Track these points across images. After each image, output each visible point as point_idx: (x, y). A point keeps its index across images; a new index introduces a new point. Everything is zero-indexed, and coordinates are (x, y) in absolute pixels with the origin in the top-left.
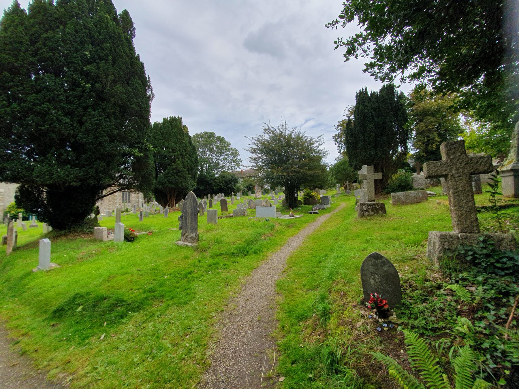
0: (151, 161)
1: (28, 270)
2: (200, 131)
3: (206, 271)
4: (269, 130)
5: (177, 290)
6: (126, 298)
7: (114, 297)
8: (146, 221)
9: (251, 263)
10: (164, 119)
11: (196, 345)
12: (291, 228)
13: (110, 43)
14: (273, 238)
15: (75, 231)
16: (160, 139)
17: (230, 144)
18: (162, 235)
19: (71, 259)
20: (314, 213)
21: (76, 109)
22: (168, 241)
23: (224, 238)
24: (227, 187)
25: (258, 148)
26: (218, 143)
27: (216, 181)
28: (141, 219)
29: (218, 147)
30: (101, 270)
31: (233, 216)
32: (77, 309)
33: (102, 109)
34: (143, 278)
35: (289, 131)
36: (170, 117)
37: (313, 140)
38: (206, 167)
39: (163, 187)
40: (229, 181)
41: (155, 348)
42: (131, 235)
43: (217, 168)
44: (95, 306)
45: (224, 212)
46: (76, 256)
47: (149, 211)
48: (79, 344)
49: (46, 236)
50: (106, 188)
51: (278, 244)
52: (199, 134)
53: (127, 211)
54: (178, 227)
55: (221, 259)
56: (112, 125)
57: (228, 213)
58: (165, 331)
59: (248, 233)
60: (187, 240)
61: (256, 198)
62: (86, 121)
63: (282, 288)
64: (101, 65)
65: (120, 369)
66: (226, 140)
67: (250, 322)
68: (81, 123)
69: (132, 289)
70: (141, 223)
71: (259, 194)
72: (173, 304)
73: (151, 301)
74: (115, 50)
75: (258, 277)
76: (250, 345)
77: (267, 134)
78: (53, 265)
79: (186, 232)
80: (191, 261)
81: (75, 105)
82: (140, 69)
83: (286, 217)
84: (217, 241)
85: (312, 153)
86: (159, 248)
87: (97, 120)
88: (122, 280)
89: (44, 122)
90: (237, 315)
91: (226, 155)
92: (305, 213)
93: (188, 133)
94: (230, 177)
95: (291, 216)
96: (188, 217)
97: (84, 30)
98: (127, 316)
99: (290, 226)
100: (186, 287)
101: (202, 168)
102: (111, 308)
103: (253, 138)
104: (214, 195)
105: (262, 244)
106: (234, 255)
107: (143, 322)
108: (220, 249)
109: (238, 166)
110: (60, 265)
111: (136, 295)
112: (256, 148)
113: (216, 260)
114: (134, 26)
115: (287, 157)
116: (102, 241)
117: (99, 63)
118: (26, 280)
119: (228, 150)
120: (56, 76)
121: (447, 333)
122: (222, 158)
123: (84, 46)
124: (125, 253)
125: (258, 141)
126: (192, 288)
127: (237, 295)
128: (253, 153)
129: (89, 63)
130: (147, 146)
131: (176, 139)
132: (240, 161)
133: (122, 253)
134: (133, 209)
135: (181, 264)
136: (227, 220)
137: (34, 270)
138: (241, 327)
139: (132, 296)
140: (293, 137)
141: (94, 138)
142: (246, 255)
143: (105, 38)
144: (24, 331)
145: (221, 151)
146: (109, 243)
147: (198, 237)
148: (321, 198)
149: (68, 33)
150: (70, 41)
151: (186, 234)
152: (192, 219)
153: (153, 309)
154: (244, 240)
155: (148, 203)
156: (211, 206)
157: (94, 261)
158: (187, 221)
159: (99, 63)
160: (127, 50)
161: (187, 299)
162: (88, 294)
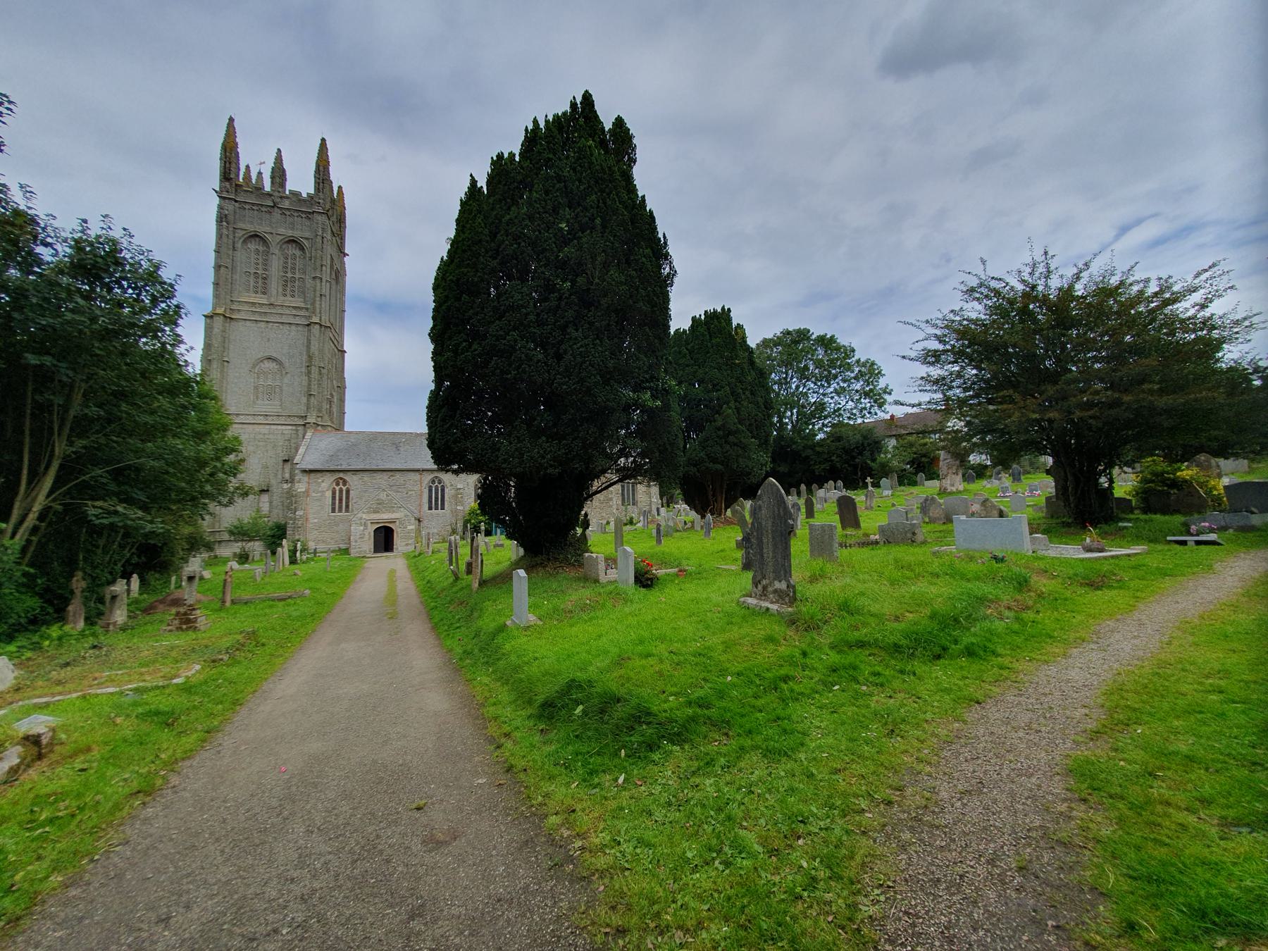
0: (677, 418)
1: (501, 620)
2: (772, 330)
3: (824, 683)
4: (982, 290)
5: (758, 715)
6: (655, 709)
7: (634, 701)
8: (670, 546)
9: (961, 683)
10: (694, 319)
11: (828, 873)
12: (1098, 588)
13: (596, 194)
14: (1029, 615)
15: (556, 559)
16: (688, 366)
17: (853, 351)
18: (706, 579)
19: (555, 610)
20: (1198, 543)
21: (551, 333)
22: (723, 595)
23: (862, 601)
24: (850, 466)
25: (948, 347)
26: (820, 351)
27: (818, 449)
28: (659, 542)
29: (819, 364)
30: (604, 639)
31: (877, 543)
32: (575, 710)
33: (589, 323)
34: (682, 672)
35: (1061, 276)
36: (706, 312)
37: (1175, 288)
38: (790, 418)
39: (698, 471)
40: (857, 448)
41: (727, 843)
42: (646, 573)
43: (820, 418)
44: (602, 711)
45: (850, 531)
46: (562, 606)
47: (671, 524)
48: (584, 780)
49: (517, 565)
50: (598, 477)
51: (1051, 637)
52: (770, 340)
53: (631, 522)
54: (740, 563)
55: (863, 658)
56: (606, 351)
57: (861, 532)
58: (743, 807)
59: (940, 593)
60: (765, 595)
61: (943, 492)
62: (566, 352)
63: (1095, 784)
64: (584, 240)
65: (662, 862)
66: (843, 340)
67: (988, 862)
68: (559, 357)
69: (664, 692)
70: (658, 549)
71: (955, 482)
72: (756, 747)
73: (704, 729)
74: (605, 203)
75: (995, 730)
76: (1002, 939)
77: (975, 303)
78: (532, 618)
79: (764, 577)
80: (783, 650)
81: (550, 327)
82: (647, 226)
83: (1071, 551)
84: (846, 608)
85: (1172, 333)
86: (707, 607)
87: (581, 346)
88: (644, 667)
89: (510, 365)
90: (937, 827)
91: (844, 381)
92: (1151, 541)
93: (746, 342)
94: (858, 437)
95: (1089, 550)
96: (765, 541)
97: (558, 186)
98: (659, 747)
99: (1095, 582)
100: (780, 712)
101: (780, 421)
102: (630, 723)
103: (927, 322)
104: (814, 486)
105: (990, 631)
106: (900, 653)
107: (694, 773)
108: (857, 629)
109: (880, 406)
110: (540, 619)
111: (669, 705)
112: (941, 347)
113: (850, 658)
114: (635, 141)
115: (1058, 360)
116: (597, 581)
117: (581, 238)
118: (499, 640)
119: (849, 368)
120: (523, 282)
121: (1109, 877)
122: (831, 389)
123: (558, 214)
124: (640, 610)
125: (947, 327)
126: (794, 717)
127: (928, 769)
128: (932, 364)
129: (566, 242)
130: (666, 383)
131: (720, 361)
132: (885, 392)
133: (635, 609)
134: (642, 518)
135: (759, 654)
136: (865, 552)
137: (507, 623)
138: (959, 870)
139: (666, 706)
140: (1079, 293)
141: (578, 382)
142: (938, 657)
143: (589, 186)
144: (506, 729)
145: (830, 372)
146: (611, 588)
147: (794, 592)
148: (1225, 487)
149: (535, 201)
150: (539, 213)
151: (764, 582)
152: (775, 546)
153: (713, 748)
154: (928, 611)
155: (668, 506)
156: (810, 513)
157: (591, 619)
158: (765, 551)
159: (581, 238)
160: (625, 196)
161: (785, 743)
162: (590, 683)
